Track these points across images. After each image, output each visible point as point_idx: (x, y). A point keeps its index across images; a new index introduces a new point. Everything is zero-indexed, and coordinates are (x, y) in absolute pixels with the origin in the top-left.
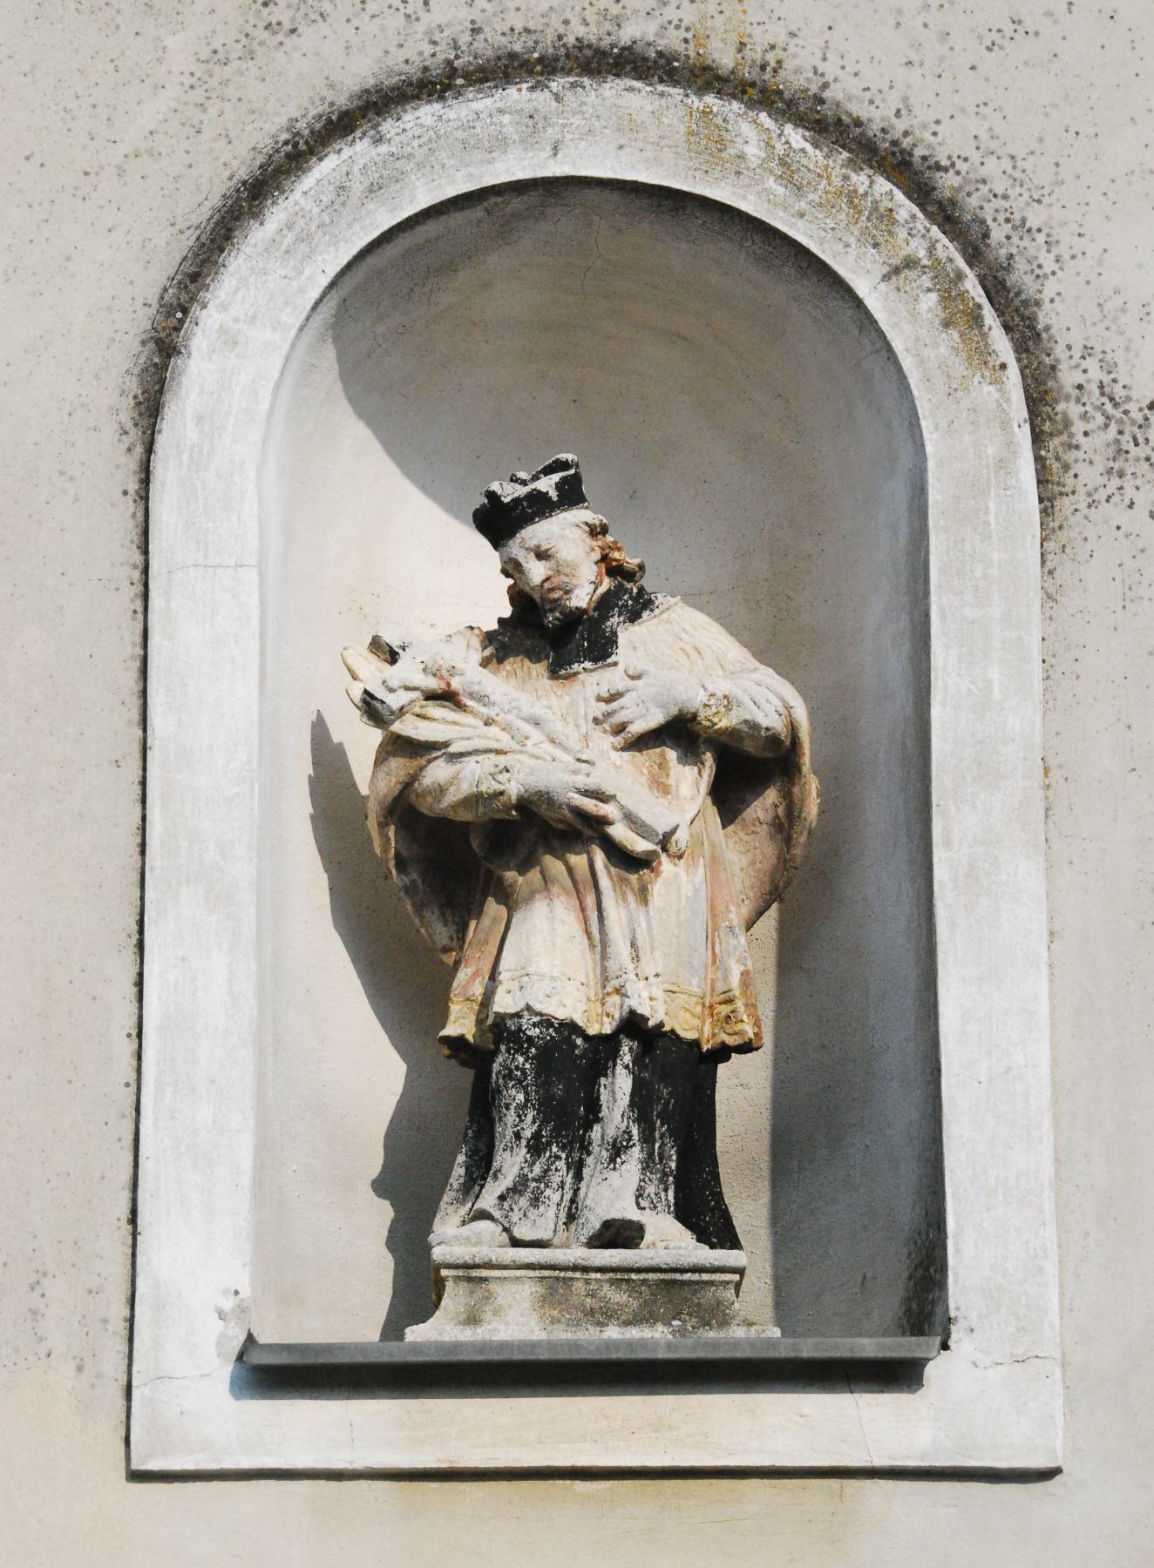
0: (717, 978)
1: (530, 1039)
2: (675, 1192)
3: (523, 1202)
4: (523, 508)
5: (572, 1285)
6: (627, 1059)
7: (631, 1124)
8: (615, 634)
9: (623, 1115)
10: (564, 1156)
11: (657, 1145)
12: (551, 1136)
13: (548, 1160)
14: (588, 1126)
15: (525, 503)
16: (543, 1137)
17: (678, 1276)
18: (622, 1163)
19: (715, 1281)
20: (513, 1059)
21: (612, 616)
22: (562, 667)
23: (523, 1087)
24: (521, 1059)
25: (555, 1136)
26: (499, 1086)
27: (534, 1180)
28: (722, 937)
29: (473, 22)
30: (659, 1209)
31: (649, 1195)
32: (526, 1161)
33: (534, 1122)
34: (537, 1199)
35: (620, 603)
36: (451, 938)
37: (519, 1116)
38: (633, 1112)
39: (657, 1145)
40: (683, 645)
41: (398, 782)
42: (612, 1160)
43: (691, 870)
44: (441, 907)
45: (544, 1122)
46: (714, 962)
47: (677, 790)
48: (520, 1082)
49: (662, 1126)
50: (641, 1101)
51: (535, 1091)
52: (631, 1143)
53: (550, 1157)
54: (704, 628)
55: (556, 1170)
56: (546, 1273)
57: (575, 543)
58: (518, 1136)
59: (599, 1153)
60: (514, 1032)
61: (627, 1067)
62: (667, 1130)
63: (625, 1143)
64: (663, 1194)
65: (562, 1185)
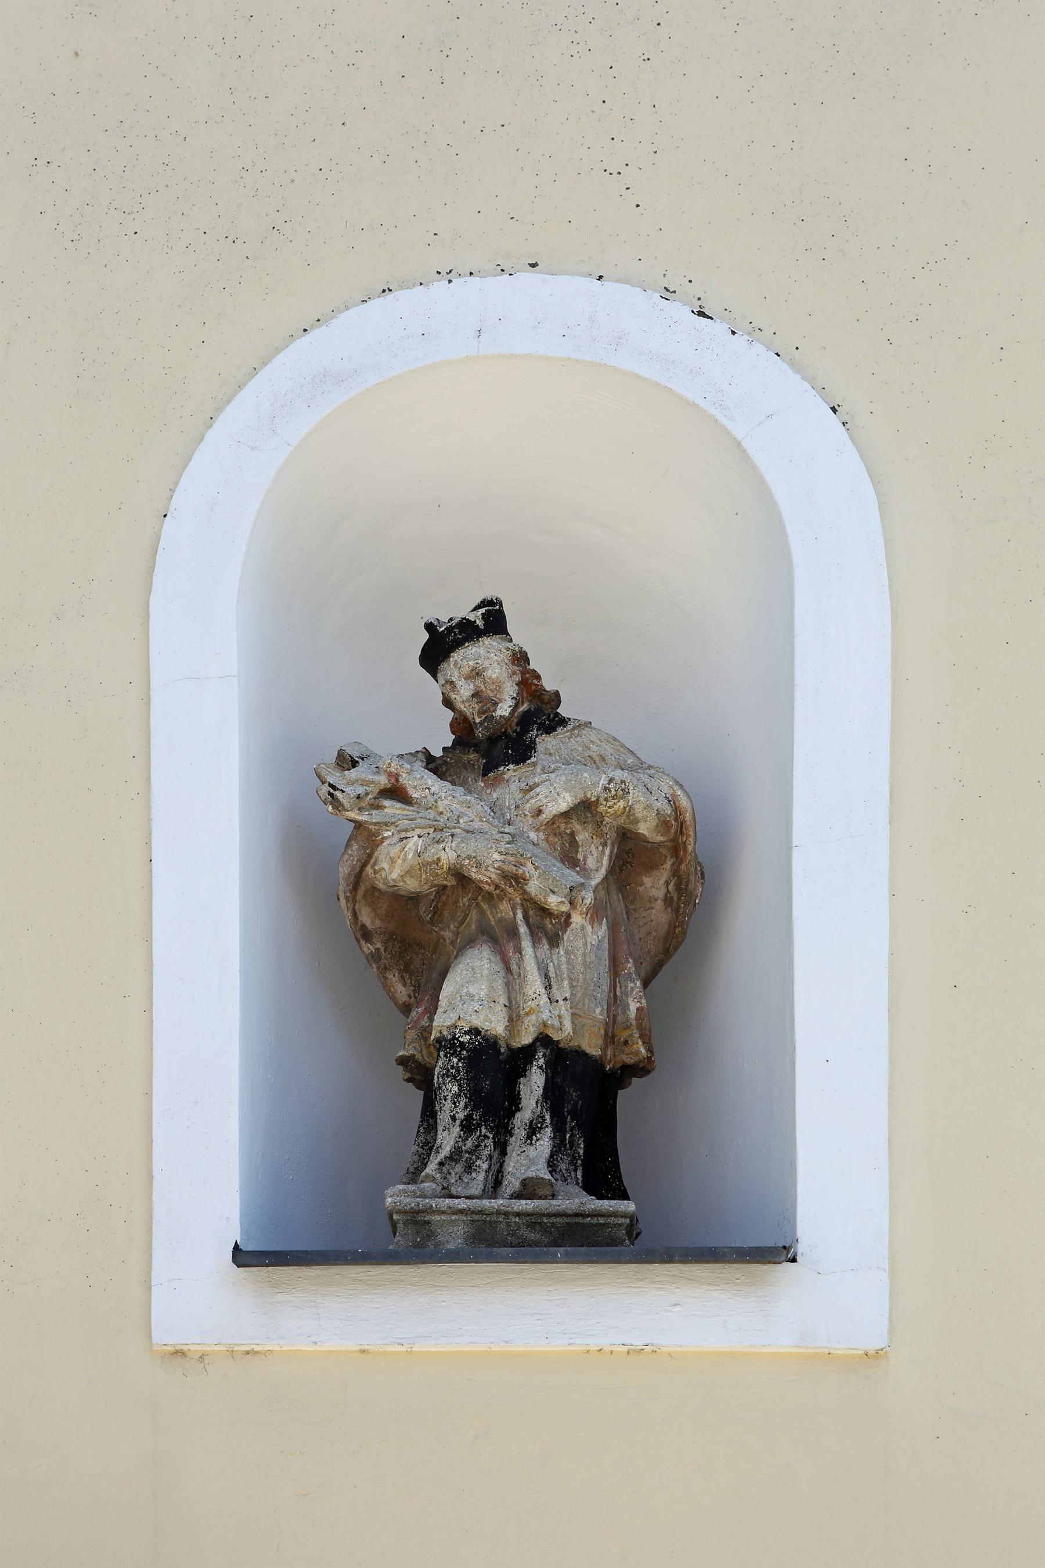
0: (618, 1014)
1: (462, 1044)
2: (583, 1173)
3: (459, 1168)
4: (455, 635)
5: (497, 1227)
6: (541, 1062)
7: (544, 1110)
8: (534, 742)
9: (537, 1102)
10: (491, 1136)
11: (568, 1136)
12: (480, 1120)
13: (478, 1138)
14: (512, 1115)
15: (457, 630)
16: (474, 1120)
17: (580, 1220)
18: (537, 1140)
19: (609, 1223)
20: (450, 1060)
21: (532, 730)
22: (490, 771)
23: (457, 1081)
24: (455, 1060)
25: (484, 1118)
26: (439, 1085)
27: (466, 1152)
28: (622, 982)
29: (303, 121)
30: (569, 1181)
31: (561, 1171)
32: (460, 1137)
33: (466, 1107)
34: (470, 1167)
35: (539, 721)
36: (410, 996)
37: (454, 1103)
38: (547, 1103)
39: (568, 1136)
40: (591, 753)
41: (358, 860)
42: (529, 1137)
43: (595, 925)
44: (400, 971)
45: (475, 1108)
46: (615, 1001)
47: (585, 864)
48: (455, 1077)
49: (572, 1121)
50: (552, 1095)
51: (467, 1084)
52: (544, 1125)
53: (480, 1136)
54: (609, 742)
55: (485, 1146)
56: (476, 1217)
57: (499, 664)
58: (453, 1118)
59: (520, 1133)
60: (450, 1040)
61: (541, 1067)
62: (577, 1124)
63: (539, 1125)
64: (573, 1173)
65: (490, 1157)
